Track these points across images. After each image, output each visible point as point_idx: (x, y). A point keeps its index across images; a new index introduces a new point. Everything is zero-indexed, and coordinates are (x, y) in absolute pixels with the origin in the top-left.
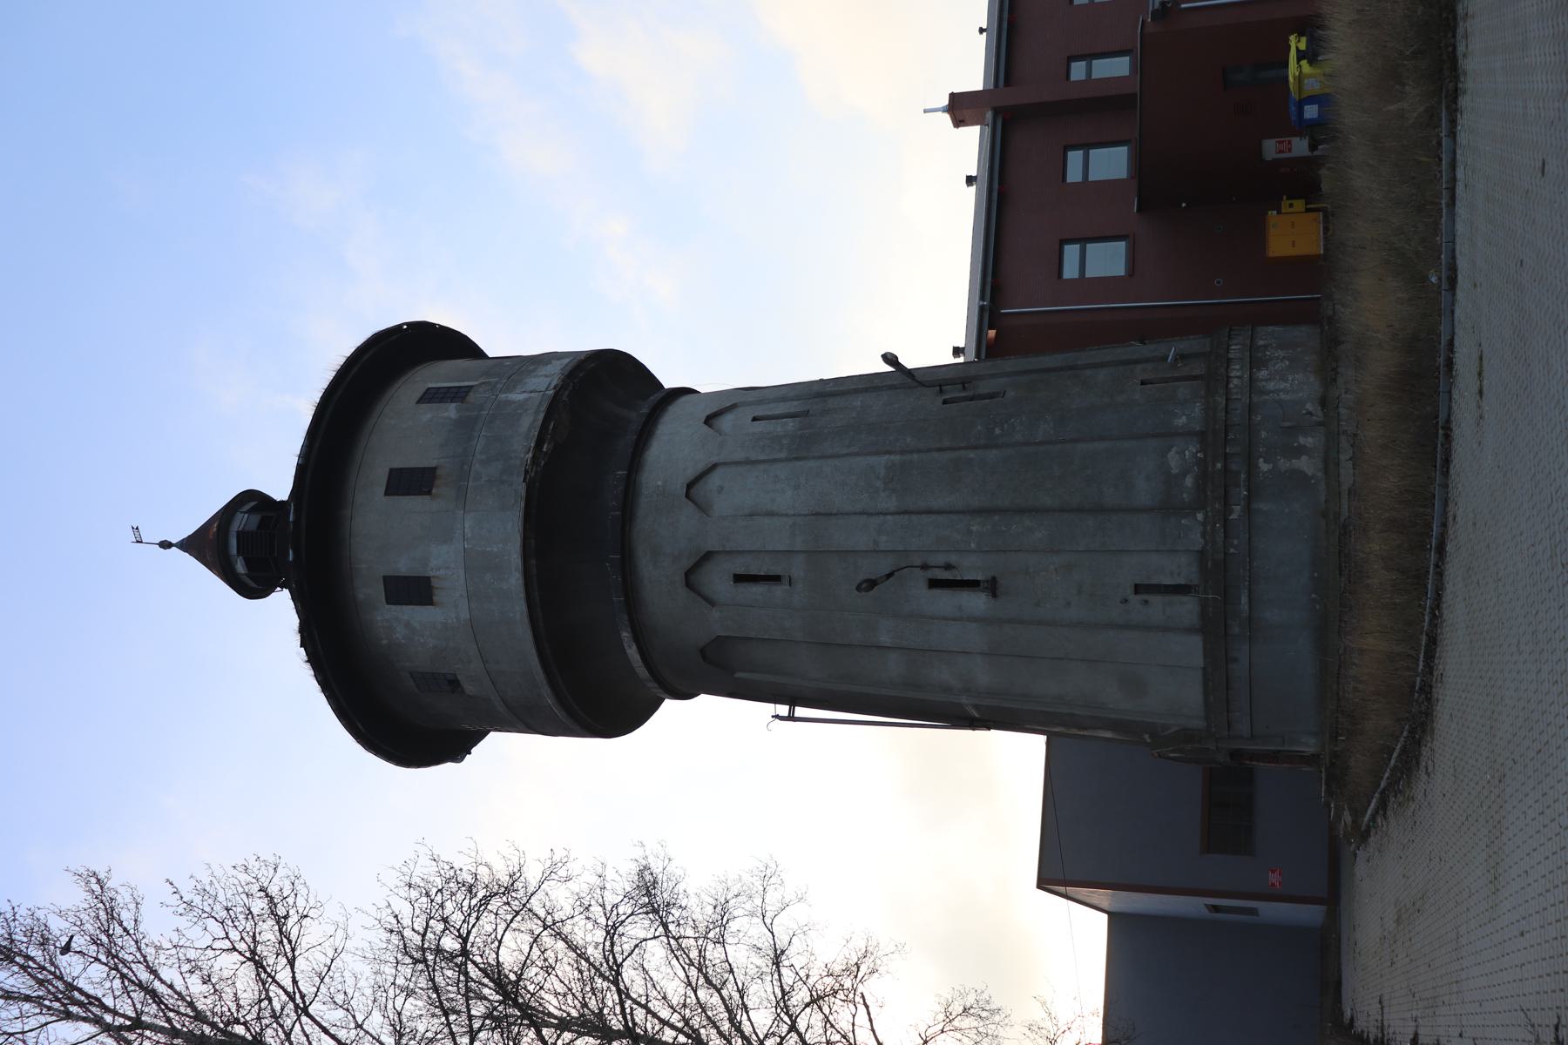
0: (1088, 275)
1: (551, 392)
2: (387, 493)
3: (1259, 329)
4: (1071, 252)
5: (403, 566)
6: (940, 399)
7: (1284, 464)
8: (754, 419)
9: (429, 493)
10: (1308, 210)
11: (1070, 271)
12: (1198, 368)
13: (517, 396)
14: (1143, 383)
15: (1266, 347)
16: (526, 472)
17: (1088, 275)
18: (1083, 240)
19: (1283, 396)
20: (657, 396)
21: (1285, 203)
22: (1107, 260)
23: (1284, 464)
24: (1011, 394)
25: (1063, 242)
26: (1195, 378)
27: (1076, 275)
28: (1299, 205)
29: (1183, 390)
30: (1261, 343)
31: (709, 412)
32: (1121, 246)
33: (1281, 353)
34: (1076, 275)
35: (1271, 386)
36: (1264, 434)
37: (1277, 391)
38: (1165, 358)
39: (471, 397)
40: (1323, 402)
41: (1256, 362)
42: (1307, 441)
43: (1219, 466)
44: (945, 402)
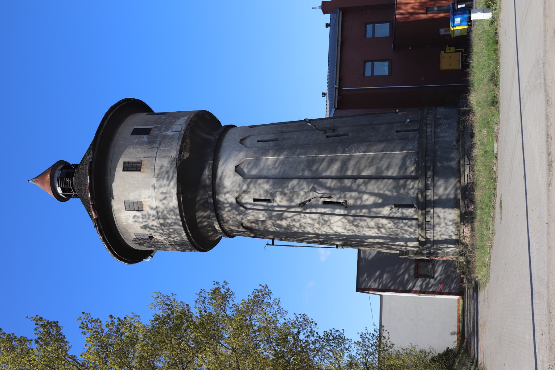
0: (375, 36)
1: (183, 132)
2: (124, 170)
3: (438, 108)
4: (368, 65)
5: (132, 197)
6: (325, 136)
7: (445, 164)
8: (258, 141)
9: (140, 170)
10: (456, 51)
11: (368, 73)
12: (417, 127)
13: (170, 133)
14: (397, 132)
15: (440, 118)
16: (177, 163)
17: (375, 36)
18: (373, 61)
19: (446, 139)
20: (220, 130)
21: (447, 48)
22: (382, 69)
23: (445, 164)
24: (350, 134)
25: (365, 62)
26: (414, 130)
27: (371, 36)
28: (453, 49)
29: (411, 135)
30: (438, 117)
31: (241, 138)
32: (387, 63)
33: (445, 122)
34: (371, 36)
35: (442, 135)
36: (439, 153)
37: (443, 137)
38: (405, 122)
39: (152, 132)
40: (458, 141)
41: (437, 125)
42: (453, 155)
43: (424, 164)
44: (327, 137)
